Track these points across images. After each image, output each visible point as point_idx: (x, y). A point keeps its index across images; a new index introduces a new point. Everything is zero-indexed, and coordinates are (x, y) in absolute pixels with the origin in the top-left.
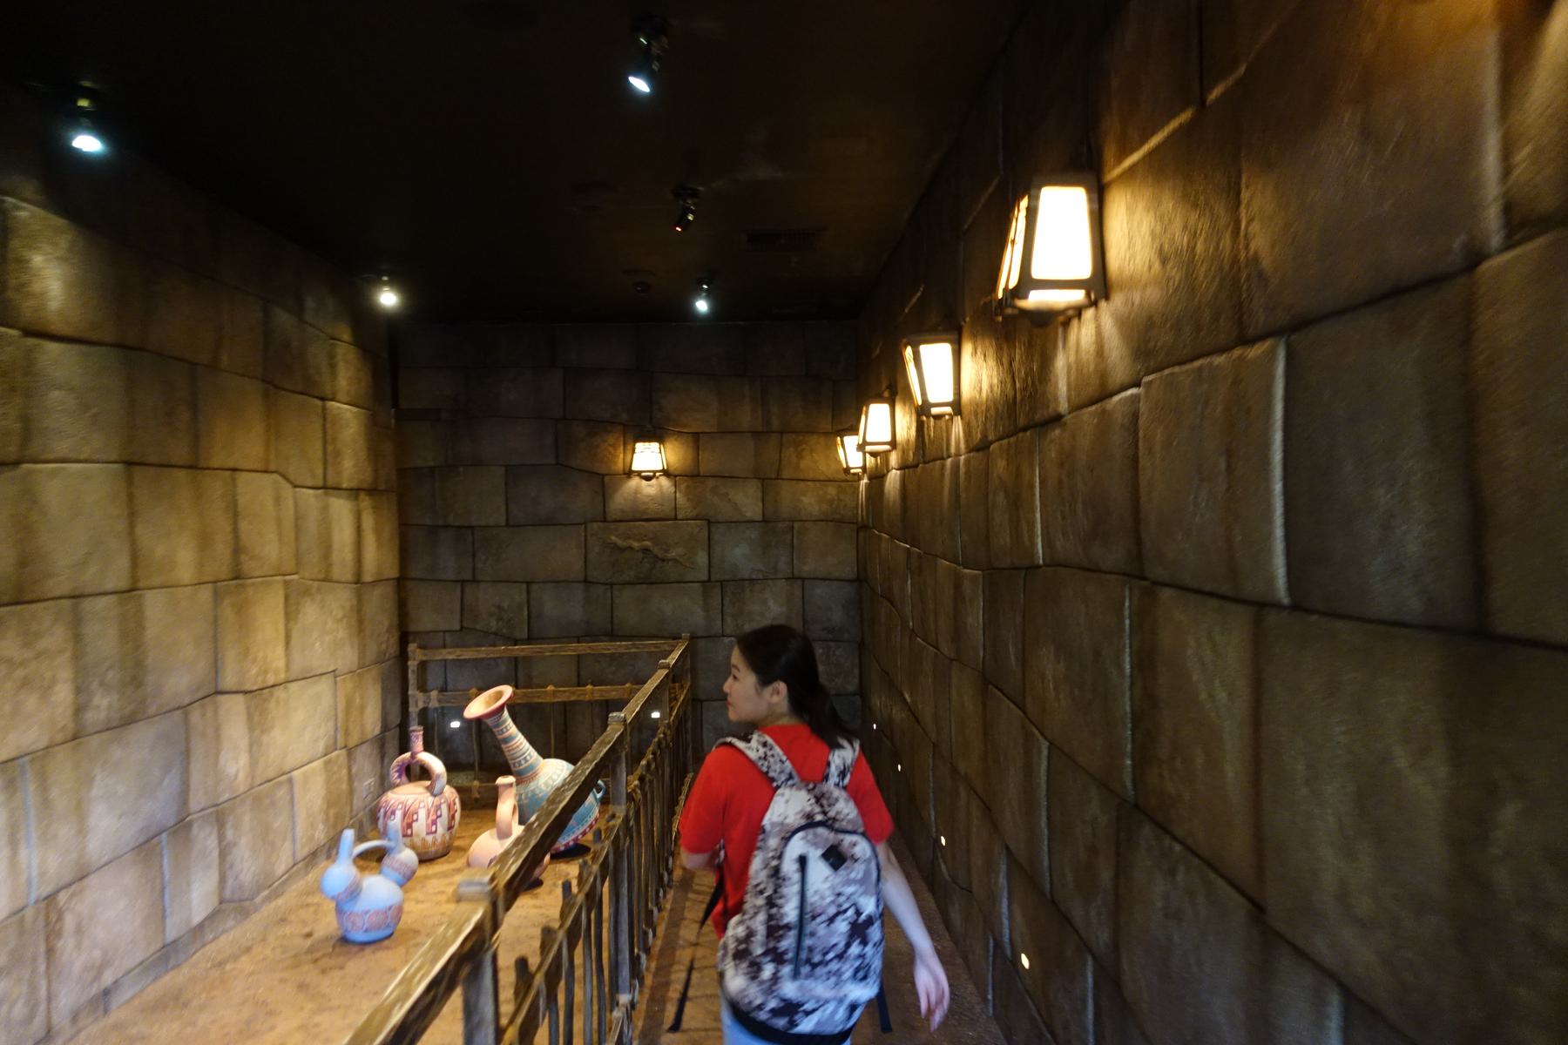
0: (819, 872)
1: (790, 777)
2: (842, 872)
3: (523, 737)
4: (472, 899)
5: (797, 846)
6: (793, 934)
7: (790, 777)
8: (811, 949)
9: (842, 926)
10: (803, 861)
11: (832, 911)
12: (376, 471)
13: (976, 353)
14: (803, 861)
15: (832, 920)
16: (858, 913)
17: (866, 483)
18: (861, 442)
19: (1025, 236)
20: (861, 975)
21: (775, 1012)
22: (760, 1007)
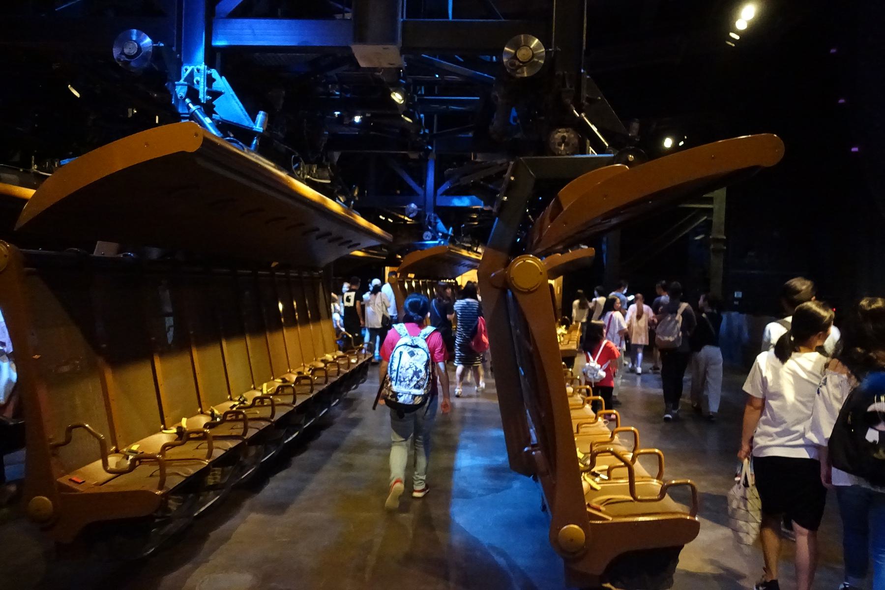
0: (406, 356)
1: (407, 335)
2: (413, 358)
3: (114, 55)
4: (206, 448)
5: (401, 349)
6: (396, 372)
7: (407, 335)
8: (400, 377)
9: (411, 372)
10: (401, 353)
11: (407, 366)
12: (465, 467)
13: (789, 369)
14: (401, 353)
15: (407, 369)
16: (416, 368)
17: (880, 489)
18: (215, 109)
19: (555, 218)
20: (417, 387)
21: (392, 396)
22: (388, 395)
